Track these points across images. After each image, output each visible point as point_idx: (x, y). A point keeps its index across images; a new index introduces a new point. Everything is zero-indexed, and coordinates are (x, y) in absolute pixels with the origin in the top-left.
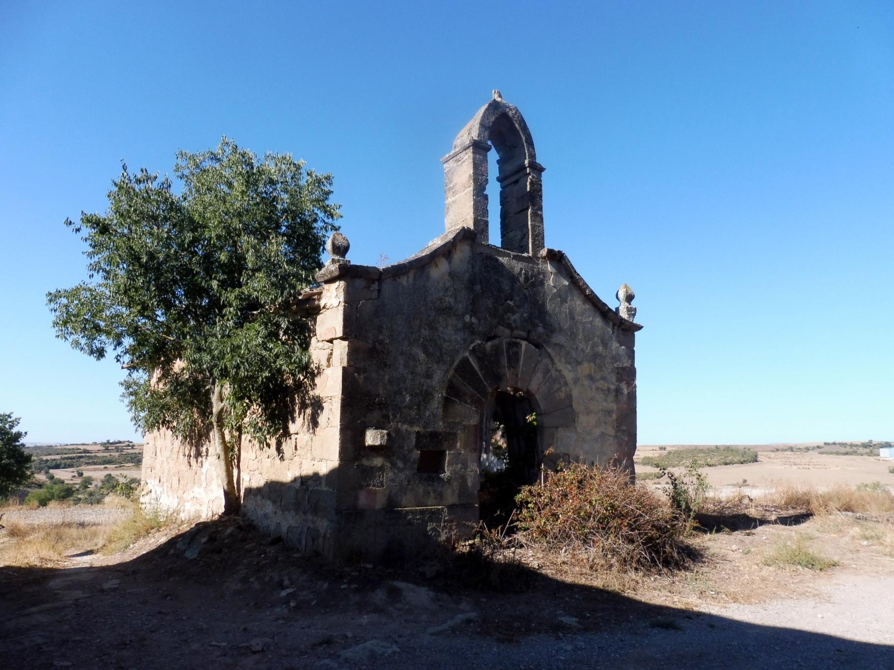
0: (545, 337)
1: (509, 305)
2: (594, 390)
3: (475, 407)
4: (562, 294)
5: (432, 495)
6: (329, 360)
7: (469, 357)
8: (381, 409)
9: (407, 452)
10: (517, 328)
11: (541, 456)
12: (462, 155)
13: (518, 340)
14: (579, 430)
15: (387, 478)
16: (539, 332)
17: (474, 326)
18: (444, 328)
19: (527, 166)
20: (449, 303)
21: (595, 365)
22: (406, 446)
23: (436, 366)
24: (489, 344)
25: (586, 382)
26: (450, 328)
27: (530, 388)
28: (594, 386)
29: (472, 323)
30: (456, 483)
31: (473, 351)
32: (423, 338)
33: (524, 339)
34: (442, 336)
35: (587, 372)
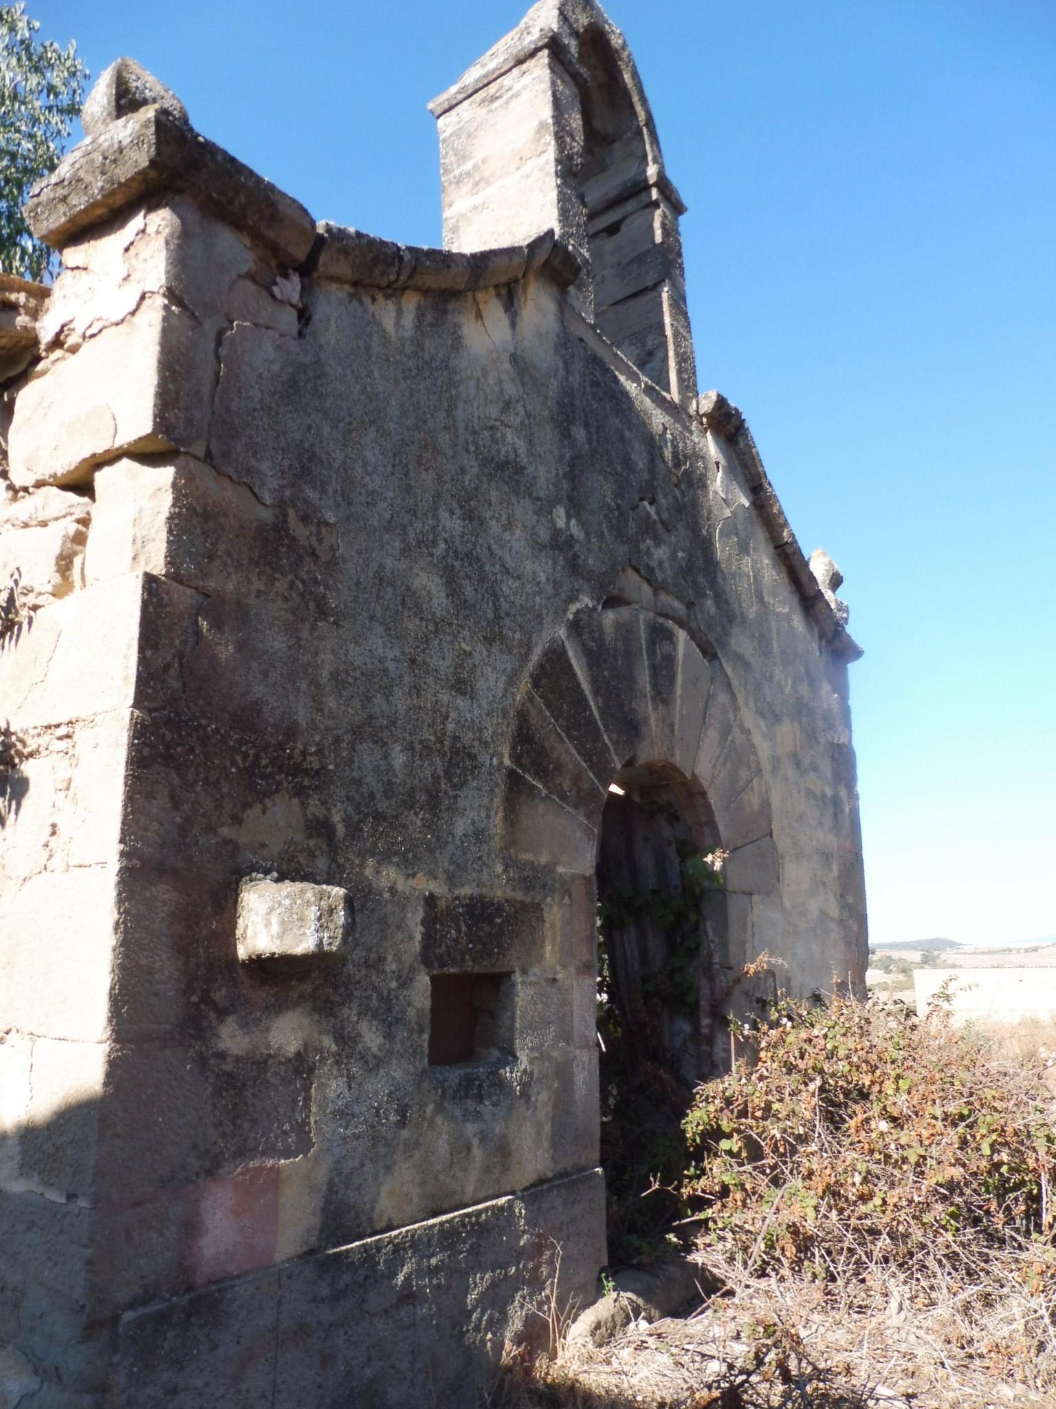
6: (64, 563)
8: (300, 792)
9: (394, 984)
11: (722, 981)
12: (506, 81)
13: (671, 622)
15: (322, 1108)
19: (651, 181)
20: (515, 451)
22: (390, 957)
30: (544, 1096)
31: (576, 627)
32: (446, 541)
33: (682, 625)
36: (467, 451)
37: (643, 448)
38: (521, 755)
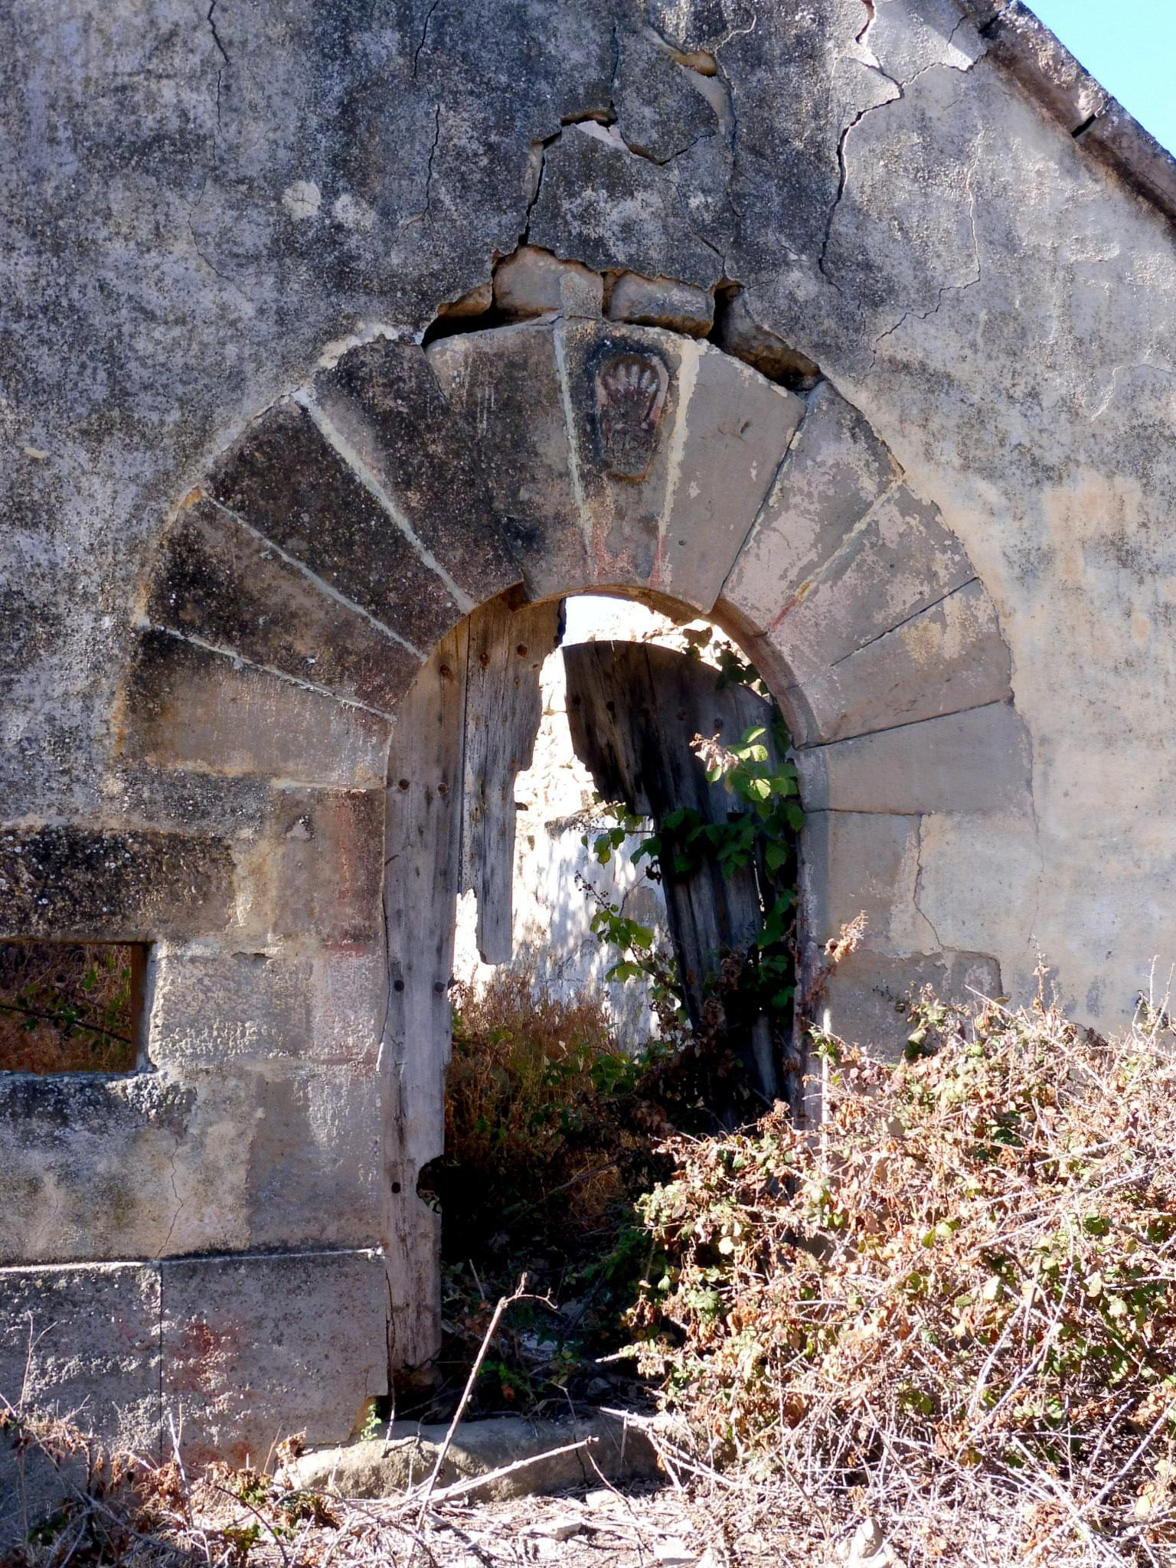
0: (830, 323)
1: (595, 144)
2: (1141, 616)
3: (361, 694)
4: (933, 113)
5: (53, 1191)
7: (317, 414)
10: (639, 267)
14: (1055, 826)
16: (792, 297)
17: (353, 242)
18: (144, 248)
20: (184, 115)
21: (1147, 487)
23: (83, 456)
24: (459, 345)
25: (1097, 577)
26: (180, 248)
27: (731, 597)
28: (1141, 598)
29: (339, 227)
34: (123, 286)
35: (1099, 521)
36: (53, 141)
37: (551, 48)
38: (179, 606)
